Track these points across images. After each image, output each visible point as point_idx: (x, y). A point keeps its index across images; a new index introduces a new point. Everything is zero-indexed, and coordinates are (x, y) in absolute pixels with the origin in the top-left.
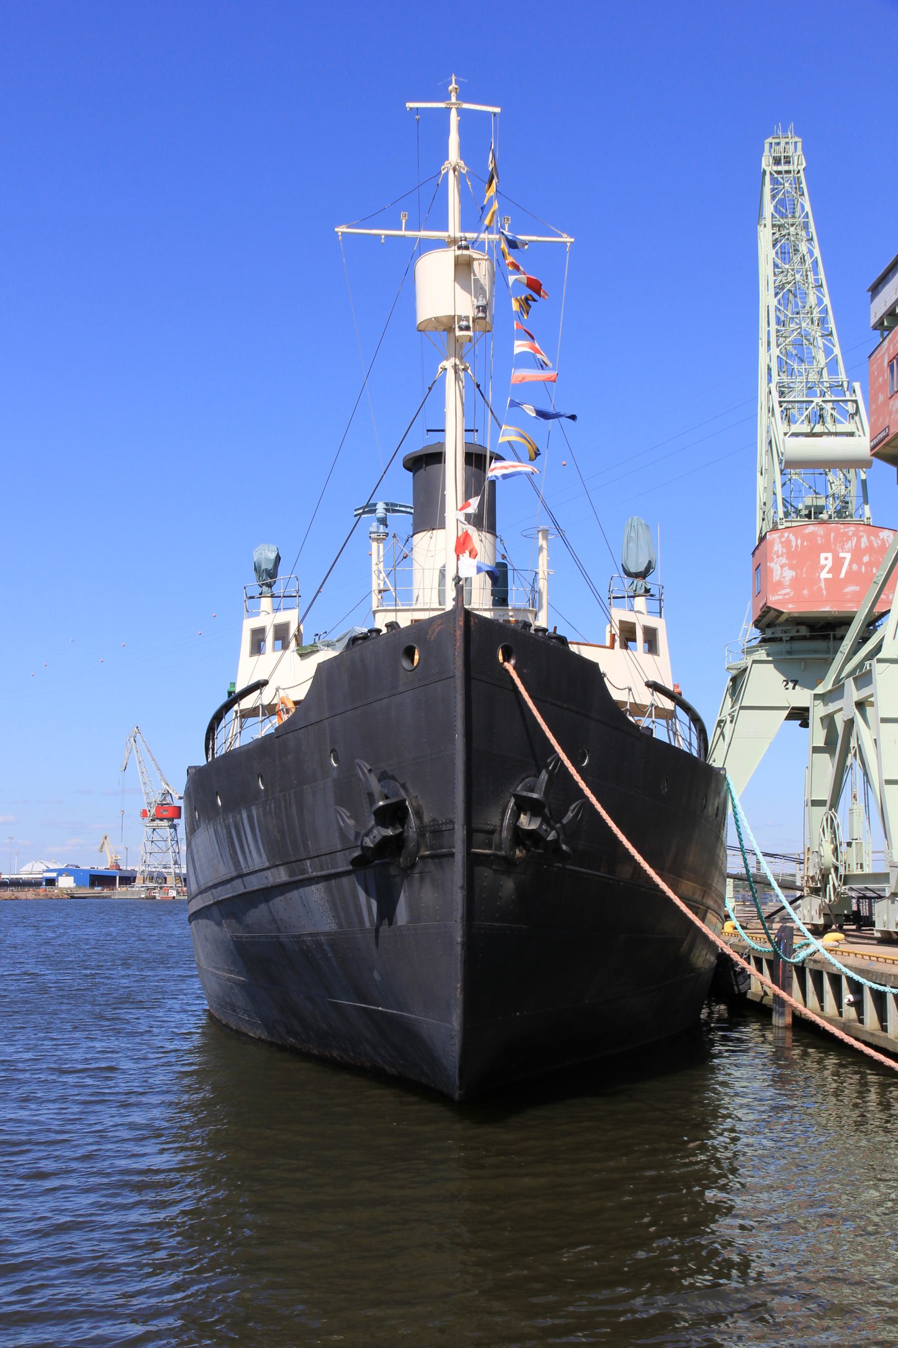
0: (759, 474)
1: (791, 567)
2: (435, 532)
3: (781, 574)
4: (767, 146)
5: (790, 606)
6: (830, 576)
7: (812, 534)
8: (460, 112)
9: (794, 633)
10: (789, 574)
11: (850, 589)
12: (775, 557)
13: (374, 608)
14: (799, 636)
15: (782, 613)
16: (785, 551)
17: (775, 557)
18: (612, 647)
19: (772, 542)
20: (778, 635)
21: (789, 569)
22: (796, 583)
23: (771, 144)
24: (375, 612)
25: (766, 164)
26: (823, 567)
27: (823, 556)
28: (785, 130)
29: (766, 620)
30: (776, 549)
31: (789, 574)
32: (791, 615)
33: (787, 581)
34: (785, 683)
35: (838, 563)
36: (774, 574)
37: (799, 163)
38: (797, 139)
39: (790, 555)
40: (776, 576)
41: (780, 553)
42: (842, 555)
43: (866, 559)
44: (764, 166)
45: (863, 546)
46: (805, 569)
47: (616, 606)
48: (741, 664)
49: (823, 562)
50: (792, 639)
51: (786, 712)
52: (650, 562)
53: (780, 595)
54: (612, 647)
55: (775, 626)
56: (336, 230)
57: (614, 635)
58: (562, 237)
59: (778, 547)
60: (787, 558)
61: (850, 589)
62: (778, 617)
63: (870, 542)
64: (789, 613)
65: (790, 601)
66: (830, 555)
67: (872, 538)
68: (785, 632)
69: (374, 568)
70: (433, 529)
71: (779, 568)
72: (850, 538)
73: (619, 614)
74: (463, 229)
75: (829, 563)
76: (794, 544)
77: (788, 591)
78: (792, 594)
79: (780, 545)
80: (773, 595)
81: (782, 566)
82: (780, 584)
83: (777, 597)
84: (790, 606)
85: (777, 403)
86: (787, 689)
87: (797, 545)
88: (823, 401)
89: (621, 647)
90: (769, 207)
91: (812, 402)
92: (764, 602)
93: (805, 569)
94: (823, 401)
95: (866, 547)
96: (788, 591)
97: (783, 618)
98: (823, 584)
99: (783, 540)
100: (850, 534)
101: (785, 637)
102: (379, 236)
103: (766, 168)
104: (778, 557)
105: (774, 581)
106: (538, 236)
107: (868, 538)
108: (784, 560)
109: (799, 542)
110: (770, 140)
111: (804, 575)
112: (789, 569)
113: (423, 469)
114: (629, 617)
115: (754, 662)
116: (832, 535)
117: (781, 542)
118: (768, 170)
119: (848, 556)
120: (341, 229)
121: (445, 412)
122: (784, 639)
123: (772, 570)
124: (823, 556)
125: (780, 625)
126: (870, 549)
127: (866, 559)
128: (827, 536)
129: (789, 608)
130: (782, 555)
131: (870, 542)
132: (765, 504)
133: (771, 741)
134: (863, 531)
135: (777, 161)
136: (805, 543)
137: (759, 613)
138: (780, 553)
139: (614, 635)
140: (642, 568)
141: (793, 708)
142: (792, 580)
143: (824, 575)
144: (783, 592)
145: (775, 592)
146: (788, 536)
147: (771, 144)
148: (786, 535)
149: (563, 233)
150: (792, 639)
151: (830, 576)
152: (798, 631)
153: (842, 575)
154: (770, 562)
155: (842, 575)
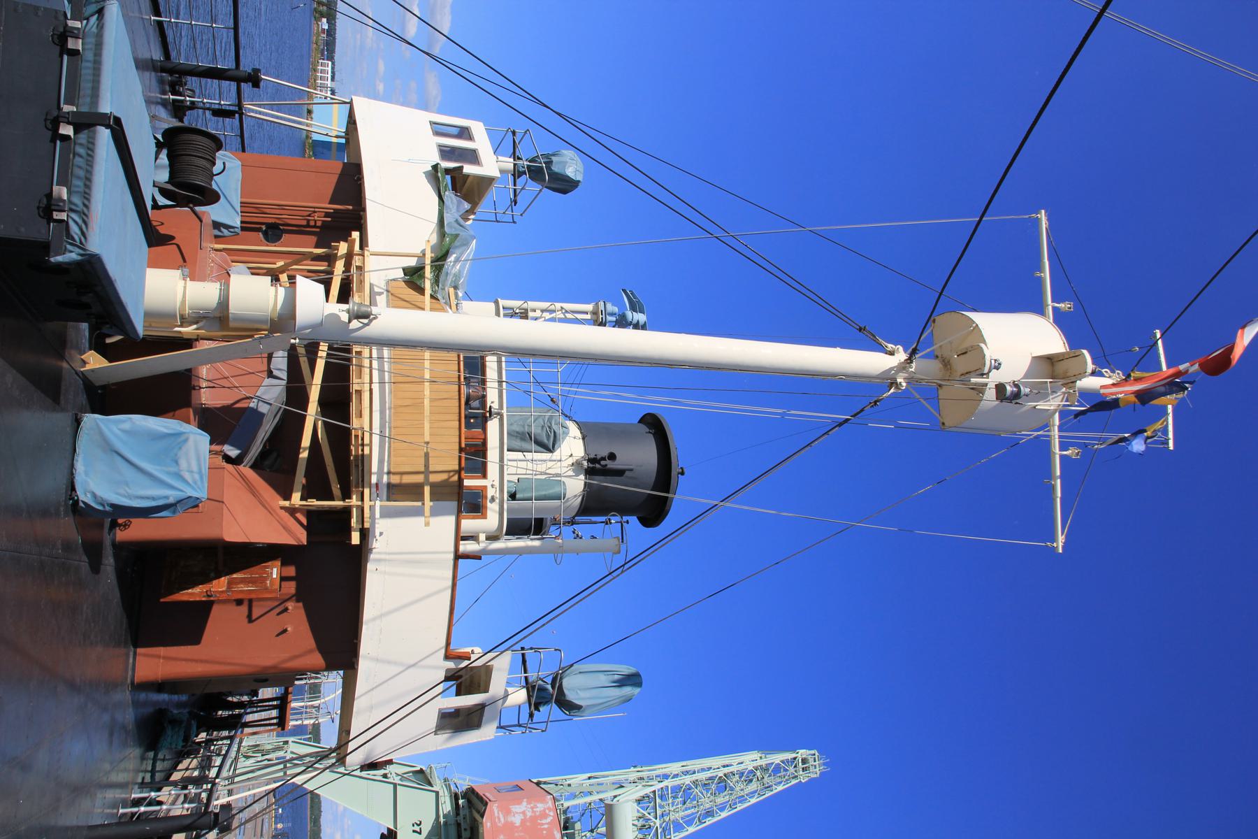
0: (589, 775)
1: (523, 822)
2: (581, 441)
3: (517, 813)
4: (813, 752)
5: (489, 824)
9: (463, 827)
10: (517, 820)
12: (532, 805)
13: (502, 302)
14: (461, 831)
15: (482, 816)
16: (537, 814)
17: (532, 805)
18: (448, 657)
19: (544, 801)
20: (461, 812)
21: (522, 820)
22: (510, 827)
23: (814, 755)
24: (496, 303)
25: (802, 753)
28: (824, 764)
29: (475, 800)
30: (538, 805)
31: (517, 820)
32: (480, 825)
33: (511, 819)
34: (419, 823)
36: (517, 806)
37: (803, 778)
38: (818, 772)
39: (534, 819)
40: (516, 808)
41: (535, 810)
44: (801, 751)
46: (522, 834)
47: (513, 661)
48: (438, 785)
50: (459, 825)
51: (392, 827)
52: (579, 707)
53: (498, 813)
54: (448, 657)
55: (470, 808)
56: (1043, 211)
57: (469, 659)
58: (1062, 535)
59: (540, 807)
60: (531, 816)
62: (478, 812)
64: (482, 823)
65: (494, 823)
68: (464, 818)
69: (558, 305)
70: (583, 439)
71: (521, 810)
73: (502, 667)
76: (544, 821)
77: (502, 820)
78: (499, 825)
79: (542, 809)
80: (498, 807)
81: (524, 813)
82: (508, 812)
83: (496, 811)
84: (489, 824)
85: (653, 789)
86: (413, 826)
87: (543, 824)
88: (657, 827)
89: (448, 670)
90: (777, 758)
91: (656, 819)
92: (492, 799)
93: (522, 834)
94: (657, 827)
96: (502, 820)
97: (477, 816)
99: (547, 811)
101: (460, 819)
102: (1041, 269)
103: (800, 754)
104: (532, 808)
105: (511, 807)
106: (1061, 498)
108: (529, 814)
109: (546, 826)
110: (817, 754)
111: (516, 834)
112: (522, 820)
113: (648, 430)
114: (497, 684)
115: (437, 793)
117: (544, 811)
118: (799, 755)
120: (1043, 215)
121: (835, 347)
122: (458, 818)
123: (519, 803)
125: (471, 812)
129: (487, 824)
130: (533, 812)
132: (569, 785)
133: (366, 815)
135: (804, 761)
136: (545, 832)
137: (481, 793)
138: (535, 810)
139: (469, 659)
140: (571, 696)
141: (396, 833)
142: (512, 824)
144: (501, 816)
145: (500, 808)
146: (550, 816)
147: (814, 755)
148: (552, 814)
149: (1066, 537)
150: (459, 825)
152: (465, 830)
154: (527, 802)
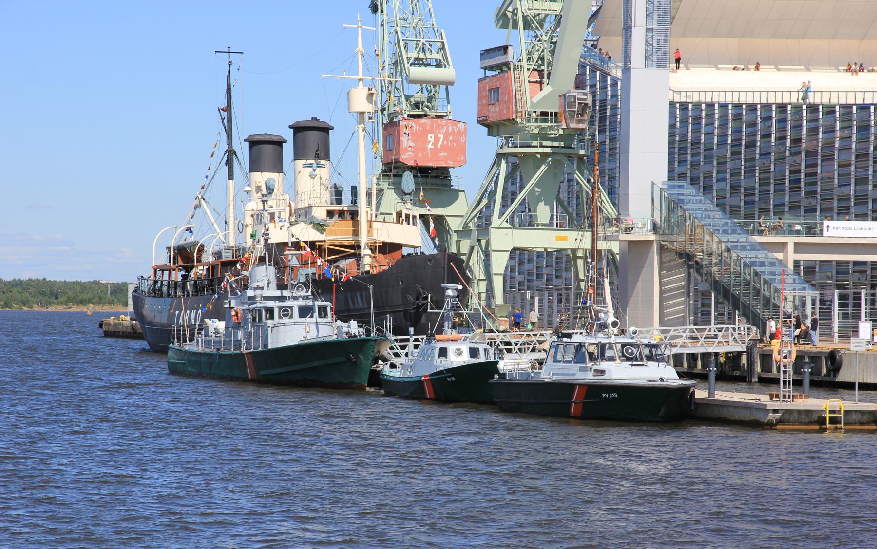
6: (433, 147)
7: (425, 123)
8: (362, 30)
11: (443, 154)
26: (430, 141)
27: (430, 135)
35: (437, 139)
42: (439, 136)
43: (451, 138)
45: (450, 131)
49: (429, 139)
61: (443, 154)
63: (453, 129)
66: (433, 136)
67: (454, 127)
72: (443, 127)
74: (363, 76)
75: (432, 140)
87: (416, 129)
95: (451, 132)
98: (429, 151)
100: (444, 124)
107: (452, 127)
109: (417, 127)
116: (435, 125)
119: (442, 136)
124: (430, 135)
126: (453, 133)
127: (451, 138)
128: (432, 125)
131: (453, 129)
134: (450, 123)
143: (430, 146)
151: (433, 147)
153: (439, 147)
155: (439, 147)
